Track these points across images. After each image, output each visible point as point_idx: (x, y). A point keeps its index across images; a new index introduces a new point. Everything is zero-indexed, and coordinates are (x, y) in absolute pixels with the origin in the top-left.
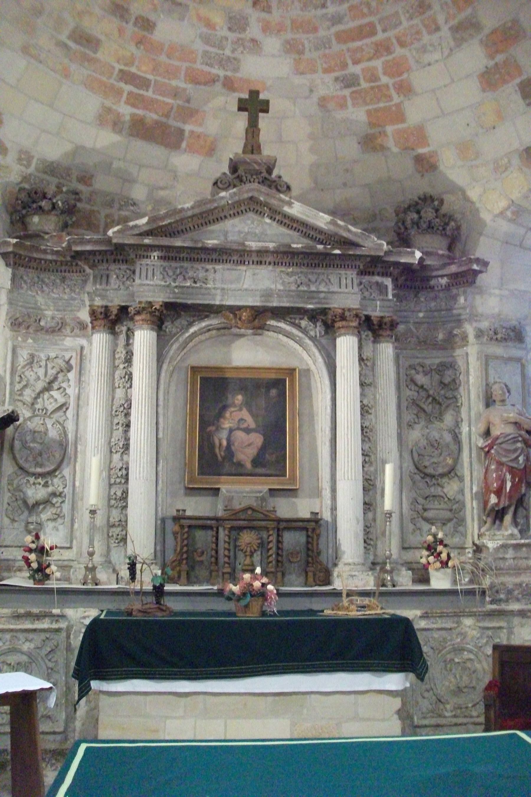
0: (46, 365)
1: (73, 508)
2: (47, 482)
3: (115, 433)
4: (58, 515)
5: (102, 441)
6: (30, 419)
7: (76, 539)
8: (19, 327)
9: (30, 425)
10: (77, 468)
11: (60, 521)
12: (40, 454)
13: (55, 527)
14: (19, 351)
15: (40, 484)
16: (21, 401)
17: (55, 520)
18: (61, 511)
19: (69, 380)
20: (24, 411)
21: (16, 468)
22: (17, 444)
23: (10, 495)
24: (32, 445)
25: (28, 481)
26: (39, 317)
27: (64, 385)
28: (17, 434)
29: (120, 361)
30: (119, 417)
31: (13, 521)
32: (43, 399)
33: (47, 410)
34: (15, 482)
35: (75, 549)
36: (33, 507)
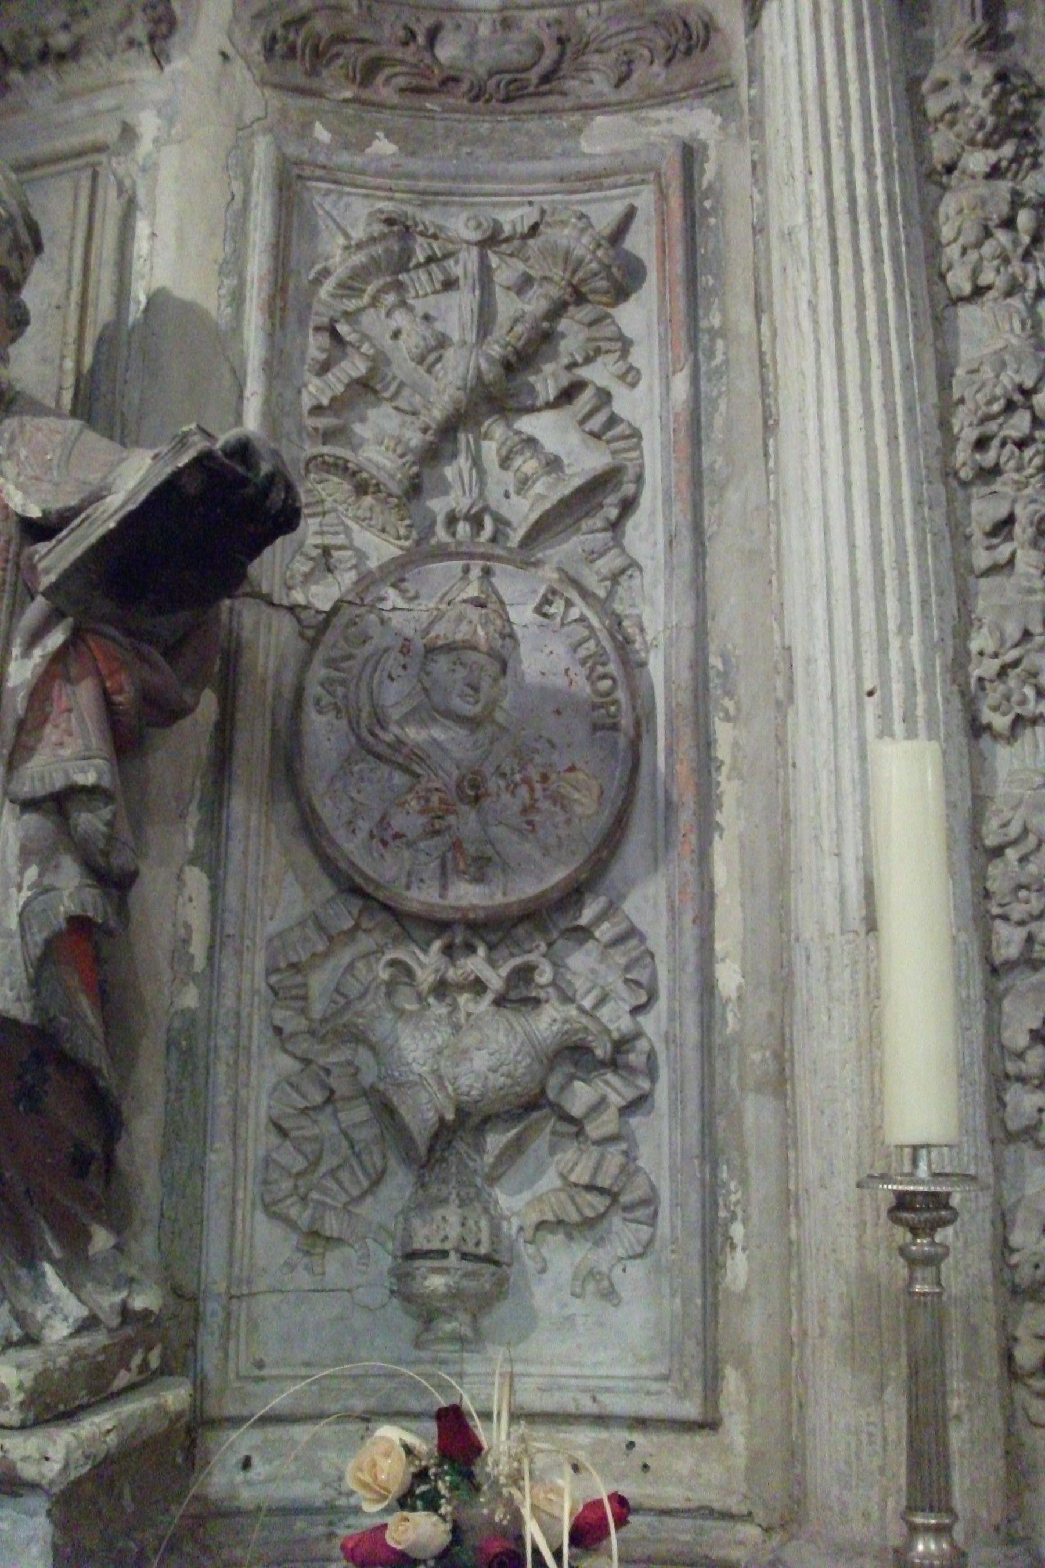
0: (485, 272)
1: (712, 1148)
2: (524, 974)
3: (988, 598)
4: (612, 1195)
5: (912, 650)
6: (396, 572)
7: (743, 1364)
8: (313, 72)
9: (403, 612)
10: (721, 873)
11: (625, 1234)
12: (473, 791)
13: (593, 1274)
14: (321, 199)
15: (478, 986)
16: (341, 467)
17: (588, 1226)
18: (629, 1169)
19: (625, 345)
20: (365, 538)
21: (327, 889)
22: (323, 734)
23: (287, 1064)
24: (414, 734)
25: (403, 970)
26: (428, 21)
27: (599, 374)
28: (318, 672)
29: (967, 125)
30: (1002, 485)
31: (315, 1239)
32: (477, 462)
33: (501, 522)
34: (319, 982)
35: (736, 1428)
36: (447, 1145)
